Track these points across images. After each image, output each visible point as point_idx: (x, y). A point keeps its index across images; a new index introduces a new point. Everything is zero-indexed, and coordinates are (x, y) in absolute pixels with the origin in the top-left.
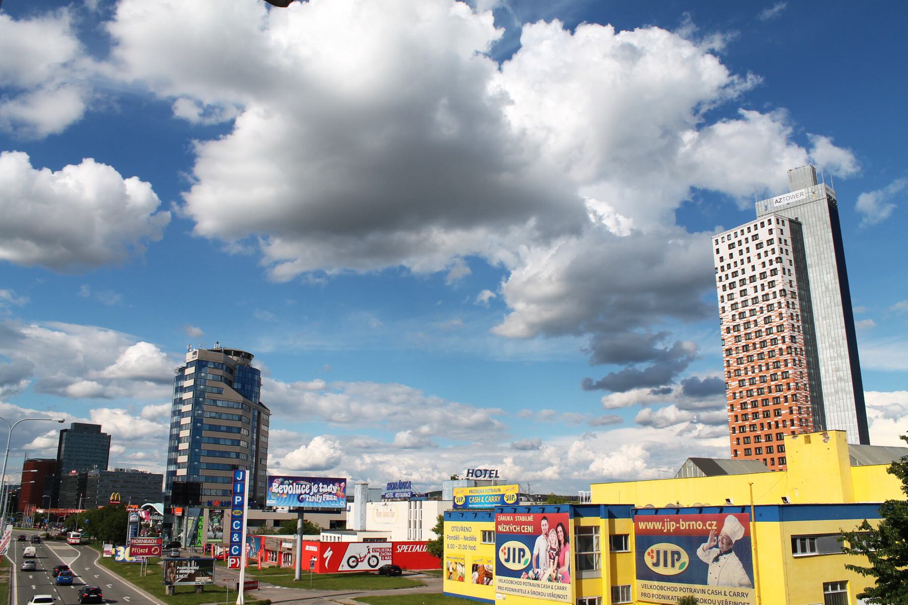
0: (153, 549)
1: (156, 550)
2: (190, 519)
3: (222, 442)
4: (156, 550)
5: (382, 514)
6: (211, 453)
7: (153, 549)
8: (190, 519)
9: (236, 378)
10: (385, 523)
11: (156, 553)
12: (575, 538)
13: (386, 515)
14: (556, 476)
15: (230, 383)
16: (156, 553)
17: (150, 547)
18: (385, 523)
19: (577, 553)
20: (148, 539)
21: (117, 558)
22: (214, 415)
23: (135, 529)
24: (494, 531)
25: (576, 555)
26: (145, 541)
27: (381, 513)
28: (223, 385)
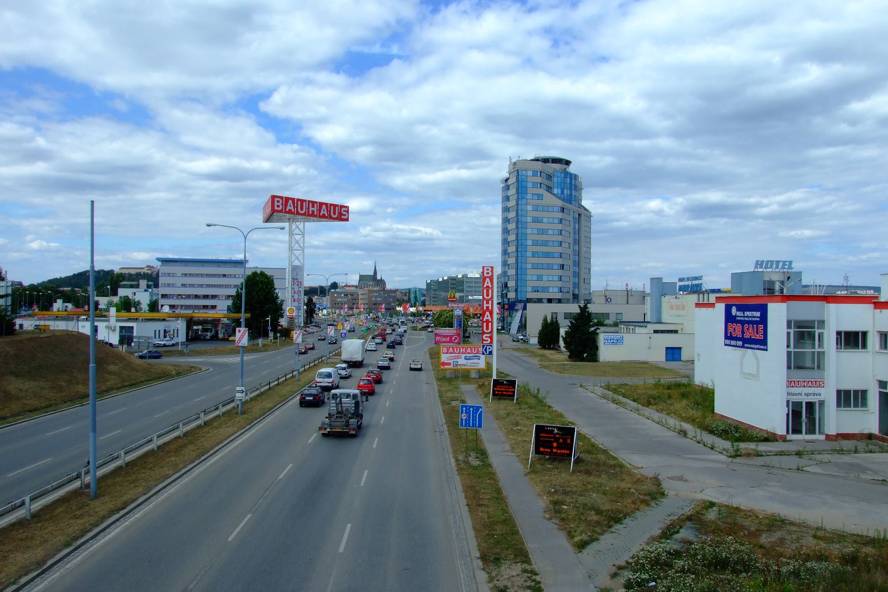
0: (453, 338)
1: (456, 339)
2: (782, 290)
3: (550, 244)
4: (456, 339)
5: (675, 307)
6: (534, 254)
7: (453, 338)
8: (782, 290)
9: (556, 184)
10: (678, 316)
11: (456, 341)
12: (788, 334)
13: (678, 308)
14: (15, 328)
15: (549, 189)
16: (456, 341)
17: (451, 337)
18: (678, 316)
19: (792, 349)
20: (449, 330)
21: (564, 336)
22: (551, 220)
23: (459, 322)
24: (443, 353)
25: (789, 353)
26: (446, 331)
27: (673, 306)
28: (542, 191)
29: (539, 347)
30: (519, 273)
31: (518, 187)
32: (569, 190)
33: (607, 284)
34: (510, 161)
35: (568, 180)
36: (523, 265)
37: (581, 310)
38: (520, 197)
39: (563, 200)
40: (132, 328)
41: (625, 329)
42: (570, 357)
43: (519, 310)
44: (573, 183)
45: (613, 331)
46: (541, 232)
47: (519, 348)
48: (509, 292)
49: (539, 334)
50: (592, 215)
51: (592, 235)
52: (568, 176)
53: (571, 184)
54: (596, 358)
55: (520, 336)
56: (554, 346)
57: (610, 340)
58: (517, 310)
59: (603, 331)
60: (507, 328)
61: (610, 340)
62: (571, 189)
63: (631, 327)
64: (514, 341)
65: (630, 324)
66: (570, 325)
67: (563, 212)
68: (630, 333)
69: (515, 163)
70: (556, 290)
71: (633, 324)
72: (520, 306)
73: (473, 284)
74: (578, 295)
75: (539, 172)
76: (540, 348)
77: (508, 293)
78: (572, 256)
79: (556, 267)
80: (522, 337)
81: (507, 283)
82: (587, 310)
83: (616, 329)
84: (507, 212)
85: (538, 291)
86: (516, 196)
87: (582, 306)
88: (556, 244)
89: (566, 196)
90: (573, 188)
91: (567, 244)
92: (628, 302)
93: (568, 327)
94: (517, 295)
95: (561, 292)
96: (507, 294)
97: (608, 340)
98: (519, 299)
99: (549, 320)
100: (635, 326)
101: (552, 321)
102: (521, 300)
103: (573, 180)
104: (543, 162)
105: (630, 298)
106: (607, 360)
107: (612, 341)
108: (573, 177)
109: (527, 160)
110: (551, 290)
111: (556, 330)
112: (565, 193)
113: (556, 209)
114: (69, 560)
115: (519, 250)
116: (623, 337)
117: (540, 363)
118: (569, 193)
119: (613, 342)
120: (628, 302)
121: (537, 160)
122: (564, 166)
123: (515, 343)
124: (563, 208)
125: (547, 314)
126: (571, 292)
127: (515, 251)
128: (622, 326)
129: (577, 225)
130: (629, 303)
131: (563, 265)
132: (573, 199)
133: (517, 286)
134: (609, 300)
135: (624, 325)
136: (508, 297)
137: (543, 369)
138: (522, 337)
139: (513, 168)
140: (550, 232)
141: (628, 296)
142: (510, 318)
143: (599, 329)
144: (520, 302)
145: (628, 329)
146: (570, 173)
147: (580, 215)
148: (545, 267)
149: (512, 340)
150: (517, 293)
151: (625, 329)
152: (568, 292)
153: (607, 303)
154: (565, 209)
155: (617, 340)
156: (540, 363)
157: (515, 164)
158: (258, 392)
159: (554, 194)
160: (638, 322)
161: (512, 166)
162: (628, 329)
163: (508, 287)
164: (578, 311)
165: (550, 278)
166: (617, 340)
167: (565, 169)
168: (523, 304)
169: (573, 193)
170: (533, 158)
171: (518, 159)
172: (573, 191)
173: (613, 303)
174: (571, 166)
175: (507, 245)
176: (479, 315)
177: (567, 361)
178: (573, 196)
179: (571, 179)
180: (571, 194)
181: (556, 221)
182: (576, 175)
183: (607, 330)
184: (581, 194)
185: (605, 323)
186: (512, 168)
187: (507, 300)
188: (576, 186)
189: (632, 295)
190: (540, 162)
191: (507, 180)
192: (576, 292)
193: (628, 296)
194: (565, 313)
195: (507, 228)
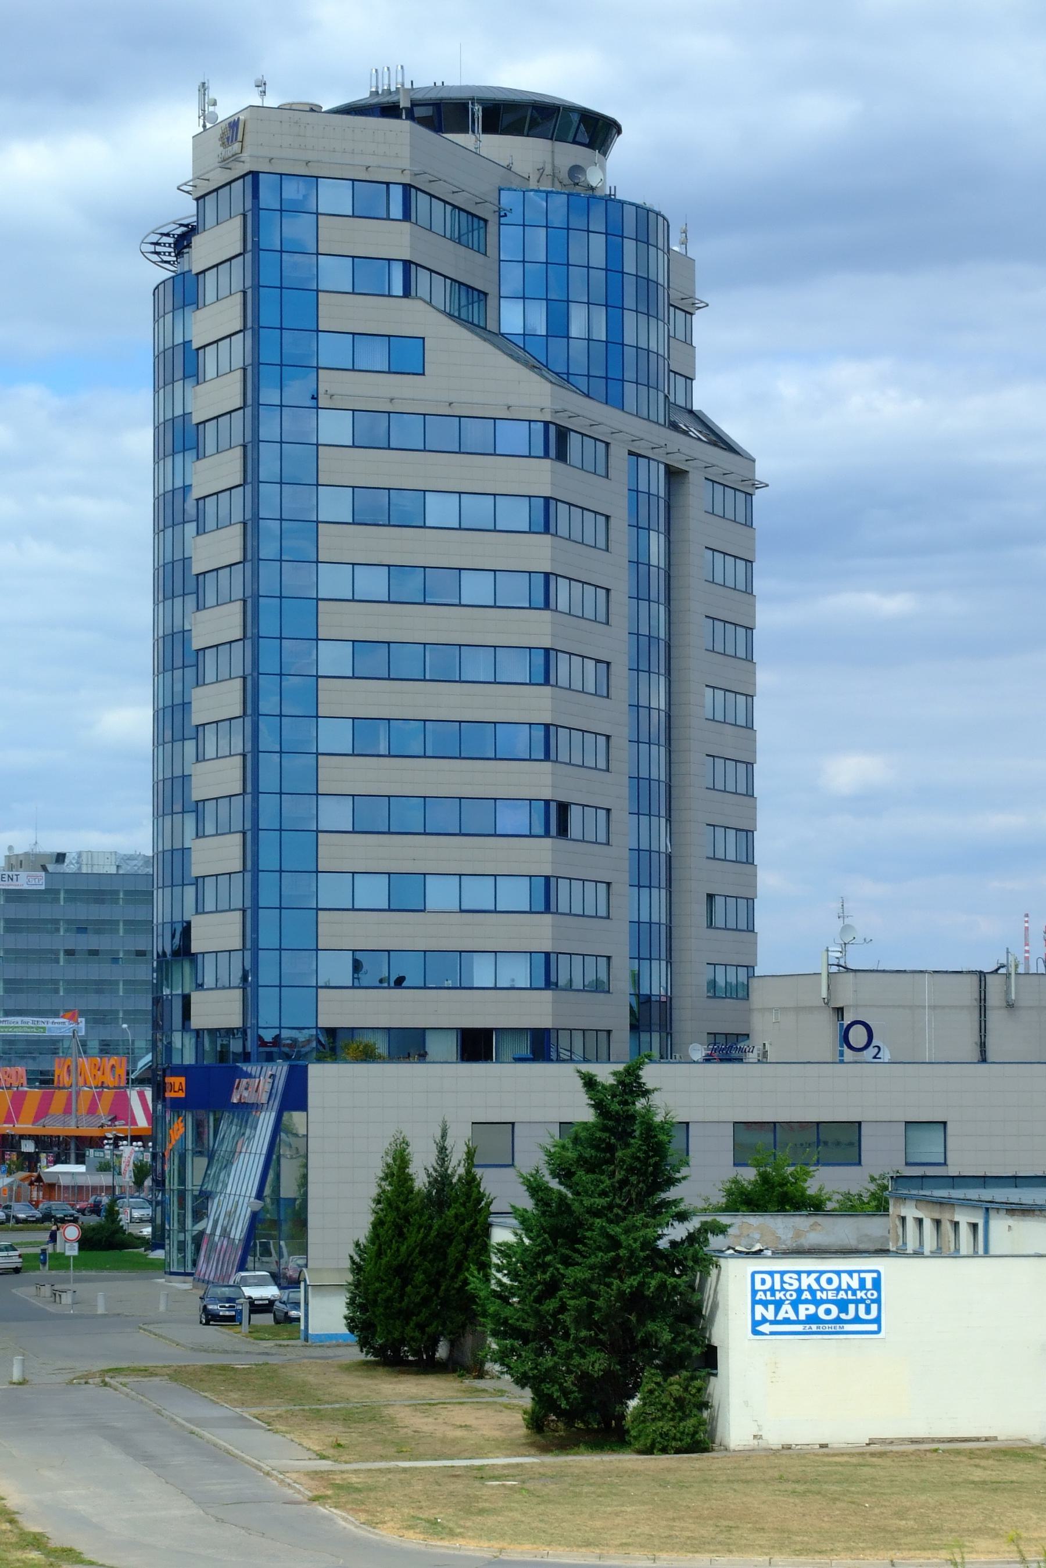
3: (478, 666)
22: (478, 510)
29: (362, 1357)
30: (268, 859)
31: (257, 287)
32: (600, 316)
33: (846, 928)
34: (203, 115)
35: (598, 242)
36: (295, 809)
37: (599, 1106)
38: (270, 354)
39: (564, 378)
40: (270, 1255)
41: (928, 1224)
42: (536, 1423)
43: (256, 1107)
44: (630, 267)
45: (852, 1243)
46: (412, 586)
47: (224, 1369)
48: (200, 986)
49: (357, 1269)
50: (761, 472)
51: (760, 608)
52: (598, 224)
53: (614, 269)
54: (712, 1435)
55: (260, 1283)
56: (453, 1345)
57: (795, 1305)
58: (247, 1110)
59: (789, 1244)
60: (183, 1229)
61: (795, 1305)
62: (613, 306)
63: (964, 1218)
64: (211, 1318)
65: (958, 1193)
66: (527, 1203)
67: (562, 456)
68: (956, 1254)
69: (234, 125)
70: (518, 972)
71: (973, 1194)
72: (265, 1085)
73: (63, 970)
74: (666, 1006)
75: (397, 193)
76: (366, 1363)
77: (196, 997)
78: (622, 751)
79: (513, 819)
80: (271, 1291)
81: (187, 930)
82: (640, 1104)
83: (873, 1227)
84: (191, 455)
85: (399, 982)
86: (238, 349)
87: (605, 1073)
88: (516, 668)
89: (578, 349)
90: (629, 302)
91: (590, 665)
92: (983, 1046)
93: (515, 1222)
94: (250, 1006)
95: (549, 984)
96: (186, 1000)
97: (778, 1305)
98: (268, 1036)
99: (420, 1182)
100: (988, 1208)
101: (441, 1181)
102: (277, 1041)
103: (629, 246)
104: (424, 122)
105: (996, 1018)
106: (774, 1439)
107: (804, 1311)
108: (630, 229)
109: (314, 109)
110: (482, 973)
111: (468, 1241)
112: (577, 329)
113: (514, 437)
114: (1007, 1555)
115: (268, 704)
116: (877, 1284)
117: (325, 1465)
118: (600, 333)
119: (813, 1319)
120: (983, 1046)
121: (389, 110)
122: (569, 154)
123: (215, 1334)
124: (563, 434)
125: (408, 1134)
126: (622, 985)
127: (237, 711)
128: (911, 1212)
129: (656, 543)
130: (991, 1056)
131: (563, 808)
132: (630, 374)
133: (256, 950)
134: (857, 1036)
135: (921, 1201)
136: (196, 1023)
137: (322, 1510)
138: (271, 1291)
139: (225, 163)
140: (477, 588)
141: (983, 1008)
142: (204, 1161)
143: (722, 1230)
144: (270, 1058)
145: (947, 1227)
146: (609, 200)
147: (674, 475)
148: (443, 817)
149: (196, 1313)
150: (256, 996)
151: (928, 1224)
152: (600, 987)
153: (849, 1054)
154: (574, 440)
155: (843, 1305)
156: (325, 1465)
157: (233, 129)
158: (256, 1462)
159: (497, 338)
160: (1015, 1181)
161: (215, 149)
162: (947, 1227)
163: (192, 957)
164: (584, 1113)
165: (478, 894)
166: (843, 1305)
167: (576, 170)
168: (281, 1069)
169: (632, 328)
170: (360, 94)
171: (257, 101)
172: (629, 318)
173: (886, 1055)
174: (619, 146)
175: (190, 673)
176: (28, 1147)
177: (510, 1447)
178: (630, 353)
179: (614, 234)
180: (614, 342)
181: (516, 514)
182: (646, 215)
183: (814, 1238)
184: (688, 342)
185: (812, 1188)
186: (213, 160)
187: (189, 1041)
188: (647, 285)
189: (1010, 1006)
190: (403, 126)
191: (183, 242)
192: (656, 985)
193: (983, 1008)
194: (741, 1127)
195: (186, 561)
